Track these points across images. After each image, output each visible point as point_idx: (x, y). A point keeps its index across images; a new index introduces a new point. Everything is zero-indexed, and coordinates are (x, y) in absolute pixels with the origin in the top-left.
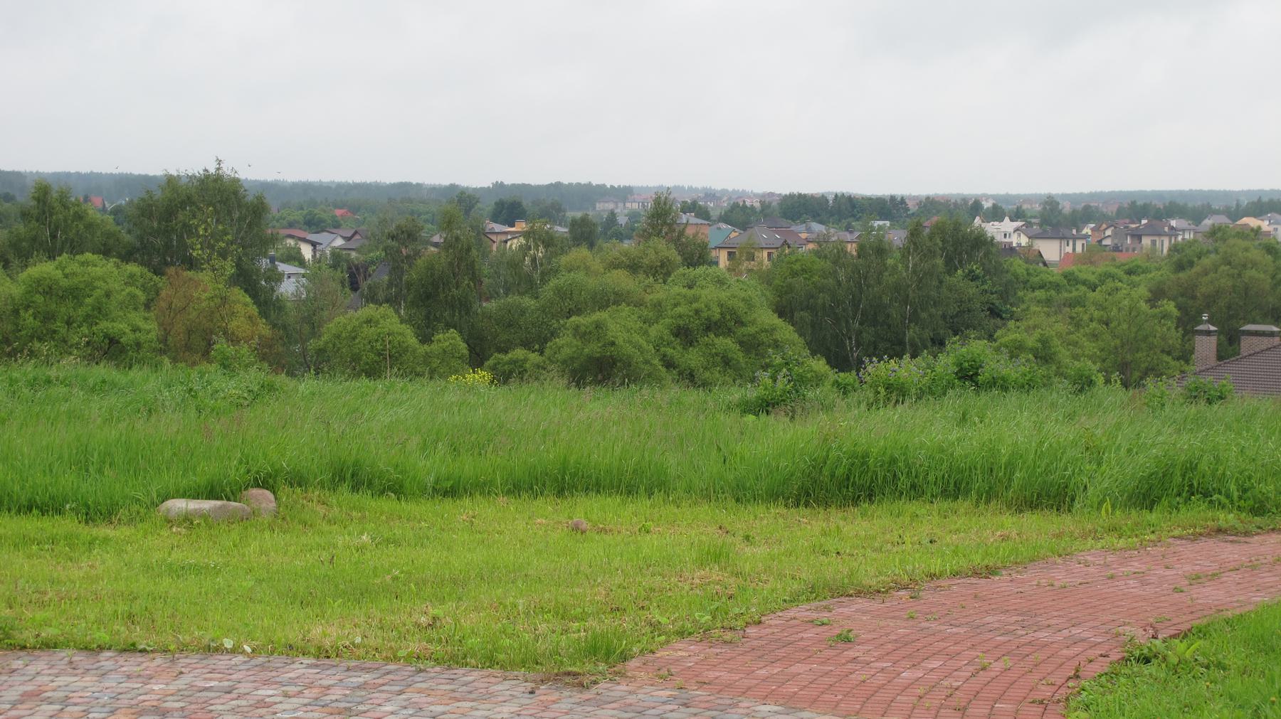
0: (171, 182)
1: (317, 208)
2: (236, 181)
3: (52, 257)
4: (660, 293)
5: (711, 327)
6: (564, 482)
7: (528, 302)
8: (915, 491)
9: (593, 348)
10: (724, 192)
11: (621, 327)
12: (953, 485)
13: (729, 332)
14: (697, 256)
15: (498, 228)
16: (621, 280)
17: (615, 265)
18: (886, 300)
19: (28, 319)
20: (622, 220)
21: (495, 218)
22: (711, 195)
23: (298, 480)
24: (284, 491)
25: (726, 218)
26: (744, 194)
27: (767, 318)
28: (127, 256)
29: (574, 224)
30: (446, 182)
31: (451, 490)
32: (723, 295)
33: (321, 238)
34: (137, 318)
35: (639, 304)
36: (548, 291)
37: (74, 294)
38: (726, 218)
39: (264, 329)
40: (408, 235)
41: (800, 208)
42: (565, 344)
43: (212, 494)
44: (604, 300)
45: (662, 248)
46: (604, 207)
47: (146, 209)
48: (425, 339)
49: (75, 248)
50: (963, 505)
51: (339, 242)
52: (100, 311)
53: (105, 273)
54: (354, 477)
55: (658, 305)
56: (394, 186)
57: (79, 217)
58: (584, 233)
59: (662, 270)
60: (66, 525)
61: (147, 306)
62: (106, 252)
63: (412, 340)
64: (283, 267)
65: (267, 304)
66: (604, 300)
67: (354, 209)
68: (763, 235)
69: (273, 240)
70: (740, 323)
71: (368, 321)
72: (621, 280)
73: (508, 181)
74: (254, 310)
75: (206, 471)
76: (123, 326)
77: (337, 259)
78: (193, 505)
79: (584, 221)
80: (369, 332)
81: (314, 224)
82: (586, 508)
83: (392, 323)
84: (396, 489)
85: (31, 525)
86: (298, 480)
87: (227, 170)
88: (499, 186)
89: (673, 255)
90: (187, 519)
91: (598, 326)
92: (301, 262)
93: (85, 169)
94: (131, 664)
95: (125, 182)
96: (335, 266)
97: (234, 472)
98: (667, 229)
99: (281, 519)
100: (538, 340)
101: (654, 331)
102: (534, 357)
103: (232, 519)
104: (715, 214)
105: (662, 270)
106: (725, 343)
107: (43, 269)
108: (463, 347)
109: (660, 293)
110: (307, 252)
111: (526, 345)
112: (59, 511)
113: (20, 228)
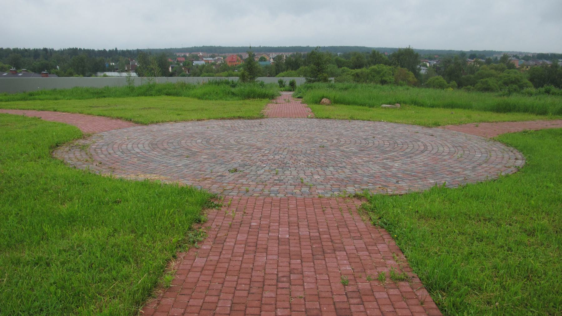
0: (399, 50)
1: (431, 55)
2: (412, 50)
3: (375, 64)
4: (502, 75)
5: (512, 82)
6: (452, 106)
7: (472, 76)
8: (519, 111)
9: (485, 86)
10: (524, 53)
11: (491, 82)
12: (526, 110)
13: (516, 84)
14: (511, 66)
15: (470, 60)
16: (493, 72)
17: (492, 69)
18: (557, 77)
19: (370, 76)
20: (499, 59)
21: (470, 58)
22: (520, 53)
23: (405, 103)
24: (402, 105)
25: (523, 59)
26: (529, 53)
27: (526, 81)
28: (390, 65)
29: (487, 60)
30: (460, 50)
31: (433, 106)
32: (516, 75)
33: (431, 62)
34: (391, 77)
35: (496, 77)
36: (476, 73)
37: (378, 73)
38: (523, 59)
39: (416, 80)
40: (449, 61)
41: (541, 56)
42: (479, 85)
43: (390, 104)
44: (489, 76)
45: (503, 65)
46: (495, 56)
47: (394, 55)
48: (448, 83)
49: (380, 63)
50: (526, 114)
51: (435, 63)
52: (384, 75)
53: (386, 68)
54: (415, 103)
55: (501, 78)
56: (427, 51)
57: (381, 57)
58: (489, 62)
59: (502, 70)
60: (367, 108)
61: (393, 75)
62: (385, 64)
63: (446, 83)
64: (422, 68)
65: (417, 74)
66: (489, 76)
67: (439, 56)
68: (531, 63)
69: (420, 62)
70: (519, 81)
71: (437, 79)
72: (493, 72)
73: (473, 50)
74: (414, 76)
75: (389, 100)
76: (388, 78)
77: (434, 65)
78: (386, 105)
79: (489, 59)
80: (437, 81)
81: (430, 59)
82: (457, 110)
83: (441, 79)
84: (422, 105)
85: (360, 107)
86: (405, 103)
87: (411, 47)
88: (472, 51)
89: (505, 66)
90: (385, 108)
91: (486, 81)
92: (427, 67)
93: (384, 47)
94: (368, 122)
95: (457, 51)
96: (433, 68)
97: (394, 101)
98: (505, 61)
99: (401, 109)
100: (473, 84)
101: (499, 83)
102: (472, 87)
103: (392, 108)
104: (520, 58)
105: (502, 70)
106: (515, 86)
107: (373, 67)
108: (456, 85)
109: (502, 75)
110: (428, 65)
111: (471, 85)
112: (365, 106)
113: (370, 59)
